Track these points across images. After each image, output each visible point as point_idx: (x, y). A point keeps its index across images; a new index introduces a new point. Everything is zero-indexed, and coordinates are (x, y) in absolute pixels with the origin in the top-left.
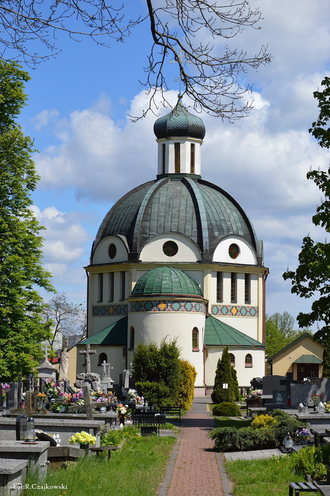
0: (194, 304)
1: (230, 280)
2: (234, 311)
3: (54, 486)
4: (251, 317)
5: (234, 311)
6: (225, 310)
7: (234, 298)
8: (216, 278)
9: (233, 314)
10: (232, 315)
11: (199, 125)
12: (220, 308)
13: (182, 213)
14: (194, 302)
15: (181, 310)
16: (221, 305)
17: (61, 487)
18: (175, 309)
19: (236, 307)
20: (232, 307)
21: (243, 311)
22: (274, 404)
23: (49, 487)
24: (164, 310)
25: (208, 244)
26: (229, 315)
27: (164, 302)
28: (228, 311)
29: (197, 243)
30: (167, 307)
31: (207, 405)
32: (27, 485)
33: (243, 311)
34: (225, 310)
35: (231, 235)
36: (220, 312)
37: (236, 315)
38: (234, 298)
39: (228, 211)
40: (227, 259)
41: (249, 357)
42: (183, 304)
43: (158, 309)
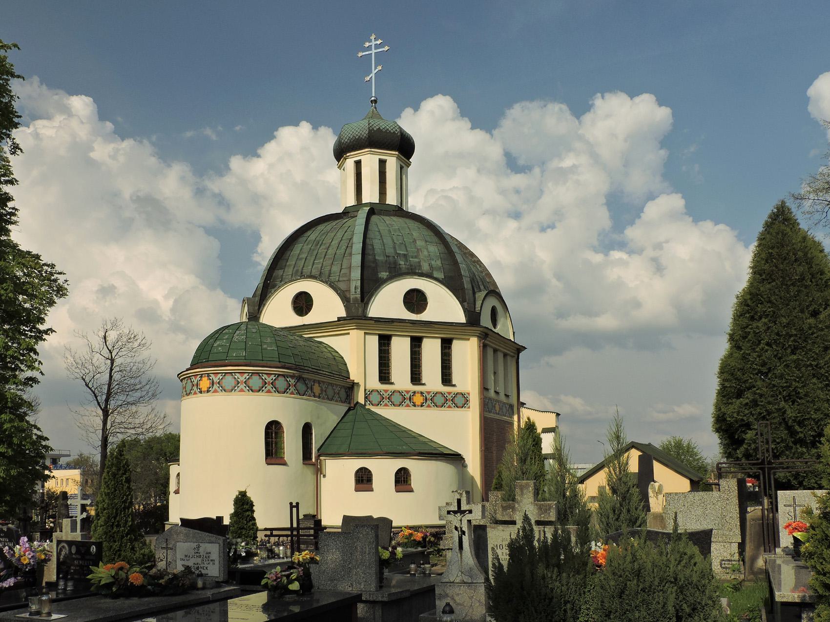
2: (418, 399)
5: (418, 399)
6: (397, 398)
7: (416, 377)
9: (416, 404)
11: (390, 129)
15: (383, 404)
18: (226, 389)
25: (360, 289)
28: (405, 400)
30: (426, 401)
31: (761, 522)
38: (416, 377)
39: (420, 243)
43: (199, 390)
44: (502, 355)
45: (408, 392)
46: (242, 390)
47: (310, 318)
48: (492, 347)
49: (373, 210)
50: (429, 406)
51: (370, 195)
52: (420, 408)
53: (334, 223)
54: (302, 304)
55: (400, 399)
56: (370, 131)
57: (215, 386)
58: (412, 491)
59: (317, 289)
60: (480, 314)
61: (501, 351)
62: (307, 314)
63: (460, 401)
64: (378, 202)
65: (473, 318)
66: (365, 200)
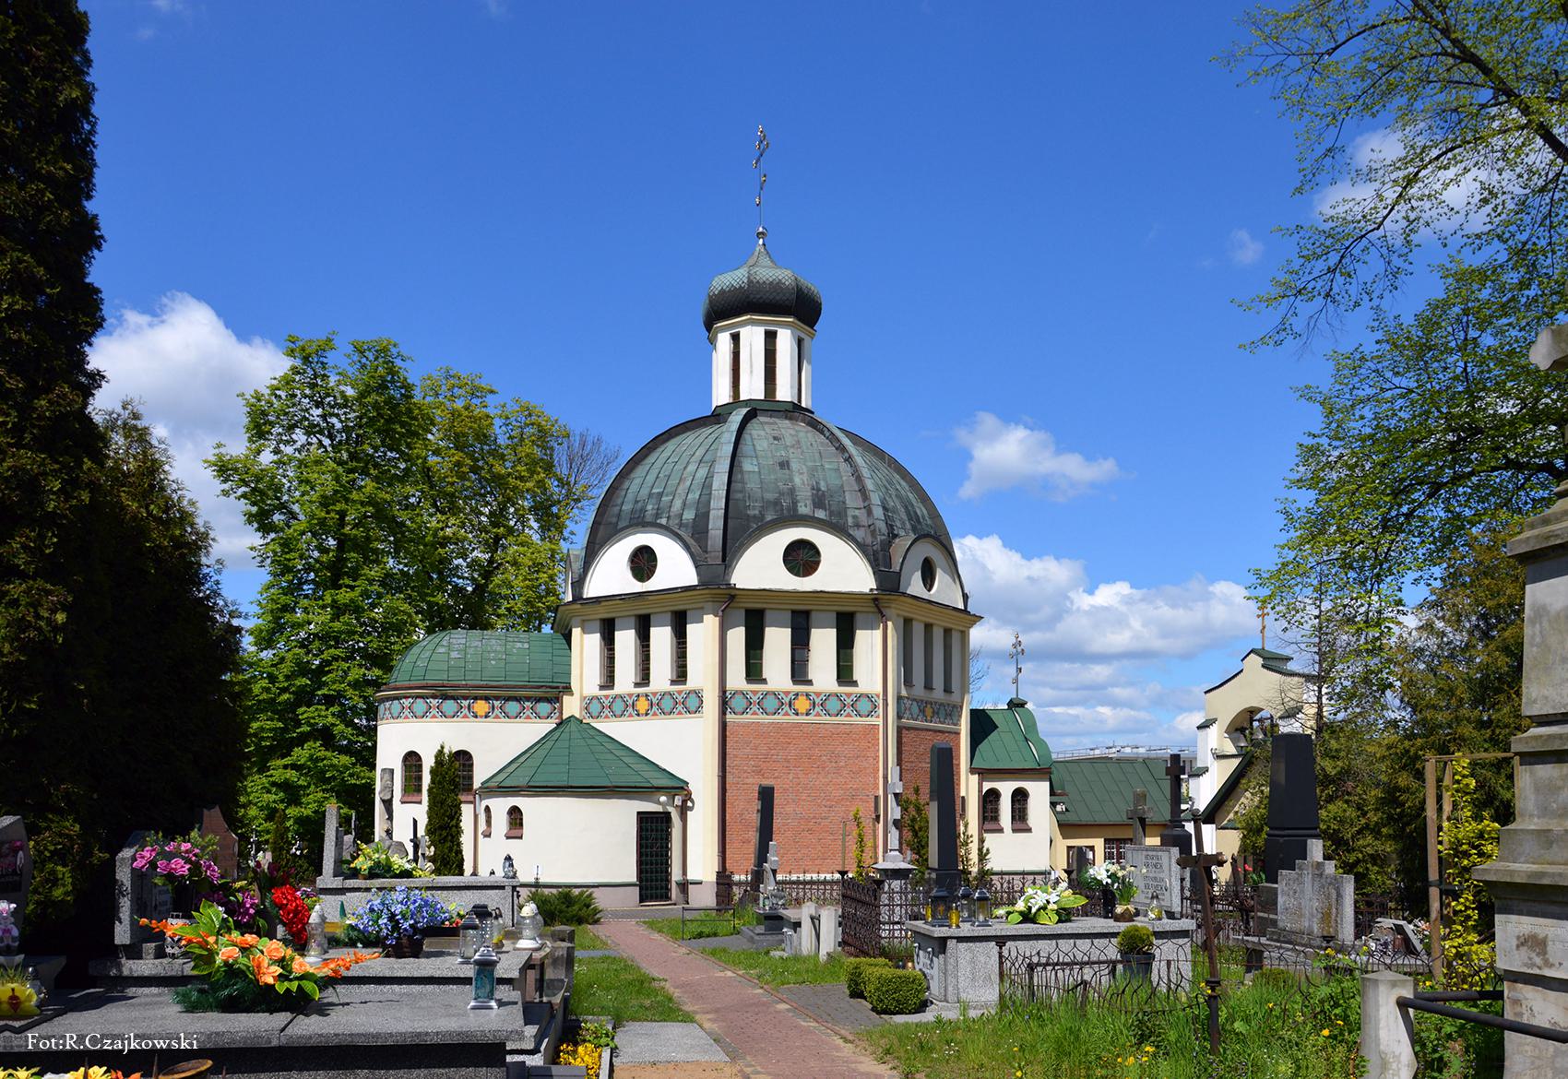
0: (406, 702)
1: (786, 634)
2: (642, 705)
3: (156, 1042)
4: (688, 715)
5: (642, 705)
6: (618, 706)
8: (788, 631)
10: (638, 715)
12: (607, 702)
13: (806, 506)
14: (406, 697)
16: (851, 694)
17: (179, 1044)
19: (647, 696)
20: (638, 696)
21: (667, 703)
22: (1266, 915)
23: (139, 1044)
24: (486, 717)
26: (631, 716)
27: (486, 698)
28: (627, 707)
29: (1028, 556)
30: (790, 702)
32: (72, 1038)
33: (667, 703)
34: (618, 706)
35: (661, 526)
36: (680, 708)
37: (647, 714)
38: (644, 677)
40: (785, 581)
41: (515, 816)
42: (465, 703)
44: (942, 631)
45: (787, 693)
46: (434, 717)
47: (655, 583)
48: (921, 621)
49: (754, 411)
50: (497, 717)
51: (753, 388)
52: (644, 717)
53: (693, 436)
54: (643, 562)
55: (829, 705)
56: (750, 282)
57: (655, 708)
58: (1029, 830)
59: (662, 545)
60: (899, 574)
61: (938, 625)
62: (649, 578)
63: (688, 704)
64: (763, 398)
65: (889, 582)
66: (743, 397)
